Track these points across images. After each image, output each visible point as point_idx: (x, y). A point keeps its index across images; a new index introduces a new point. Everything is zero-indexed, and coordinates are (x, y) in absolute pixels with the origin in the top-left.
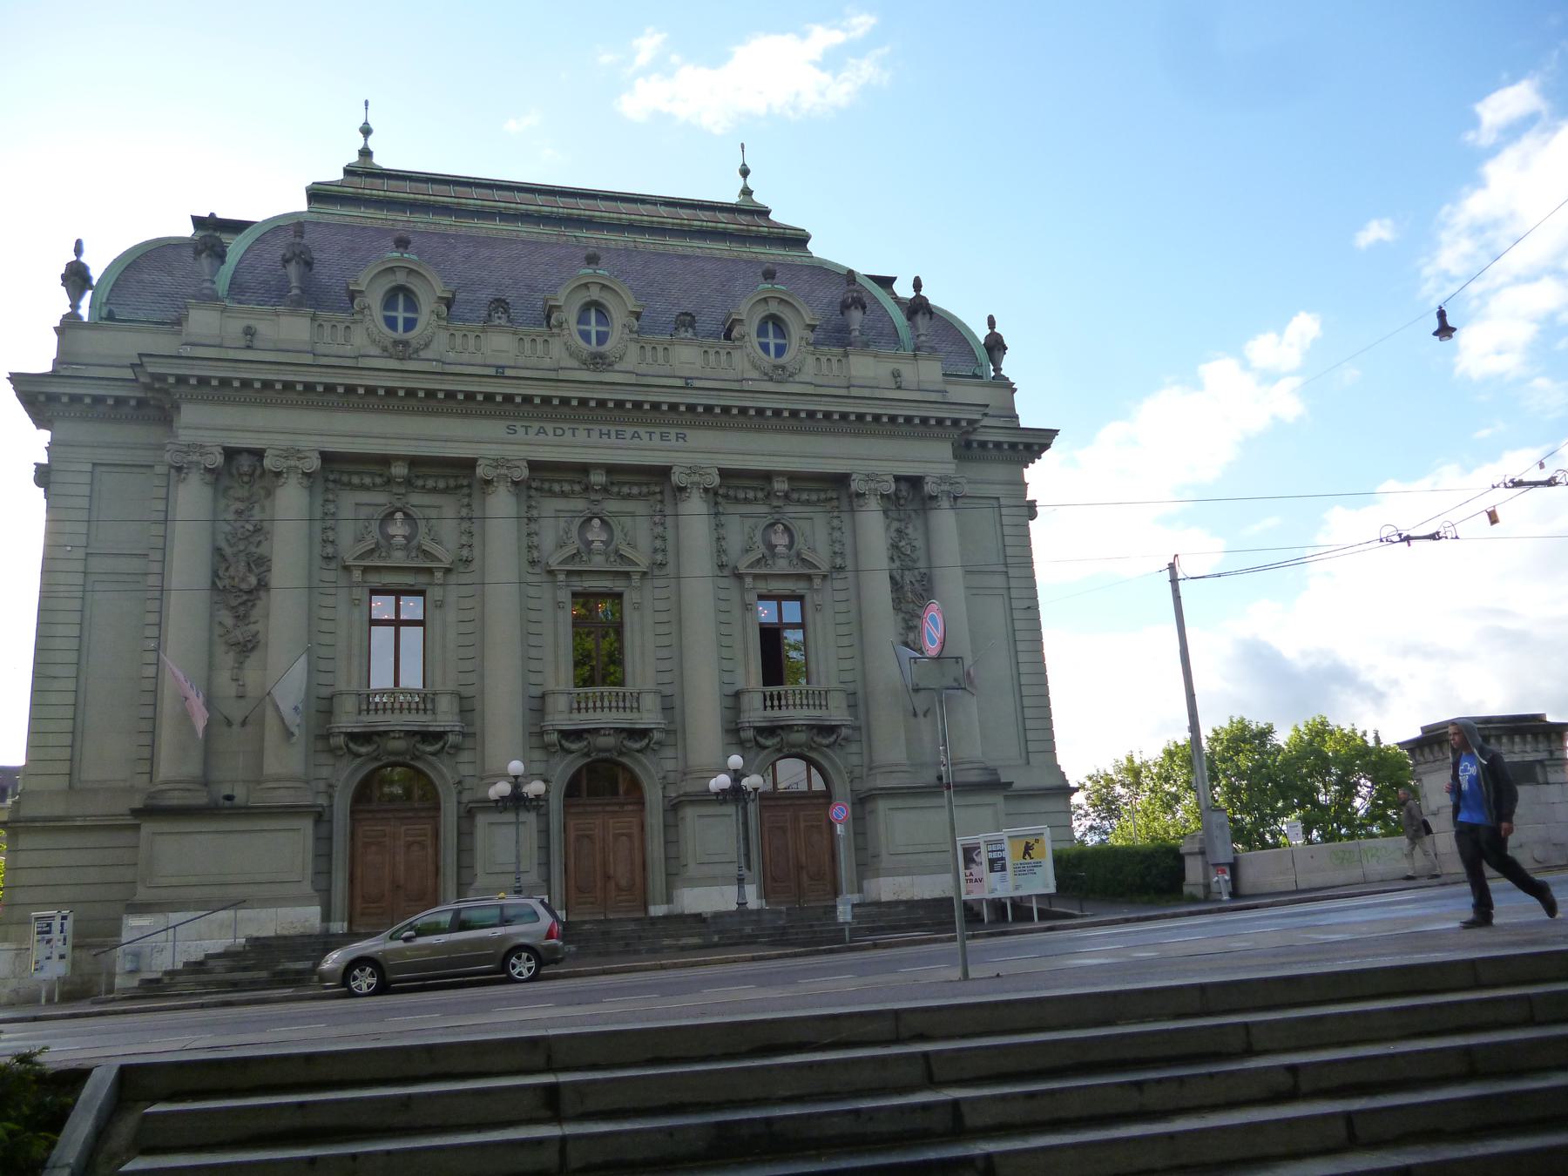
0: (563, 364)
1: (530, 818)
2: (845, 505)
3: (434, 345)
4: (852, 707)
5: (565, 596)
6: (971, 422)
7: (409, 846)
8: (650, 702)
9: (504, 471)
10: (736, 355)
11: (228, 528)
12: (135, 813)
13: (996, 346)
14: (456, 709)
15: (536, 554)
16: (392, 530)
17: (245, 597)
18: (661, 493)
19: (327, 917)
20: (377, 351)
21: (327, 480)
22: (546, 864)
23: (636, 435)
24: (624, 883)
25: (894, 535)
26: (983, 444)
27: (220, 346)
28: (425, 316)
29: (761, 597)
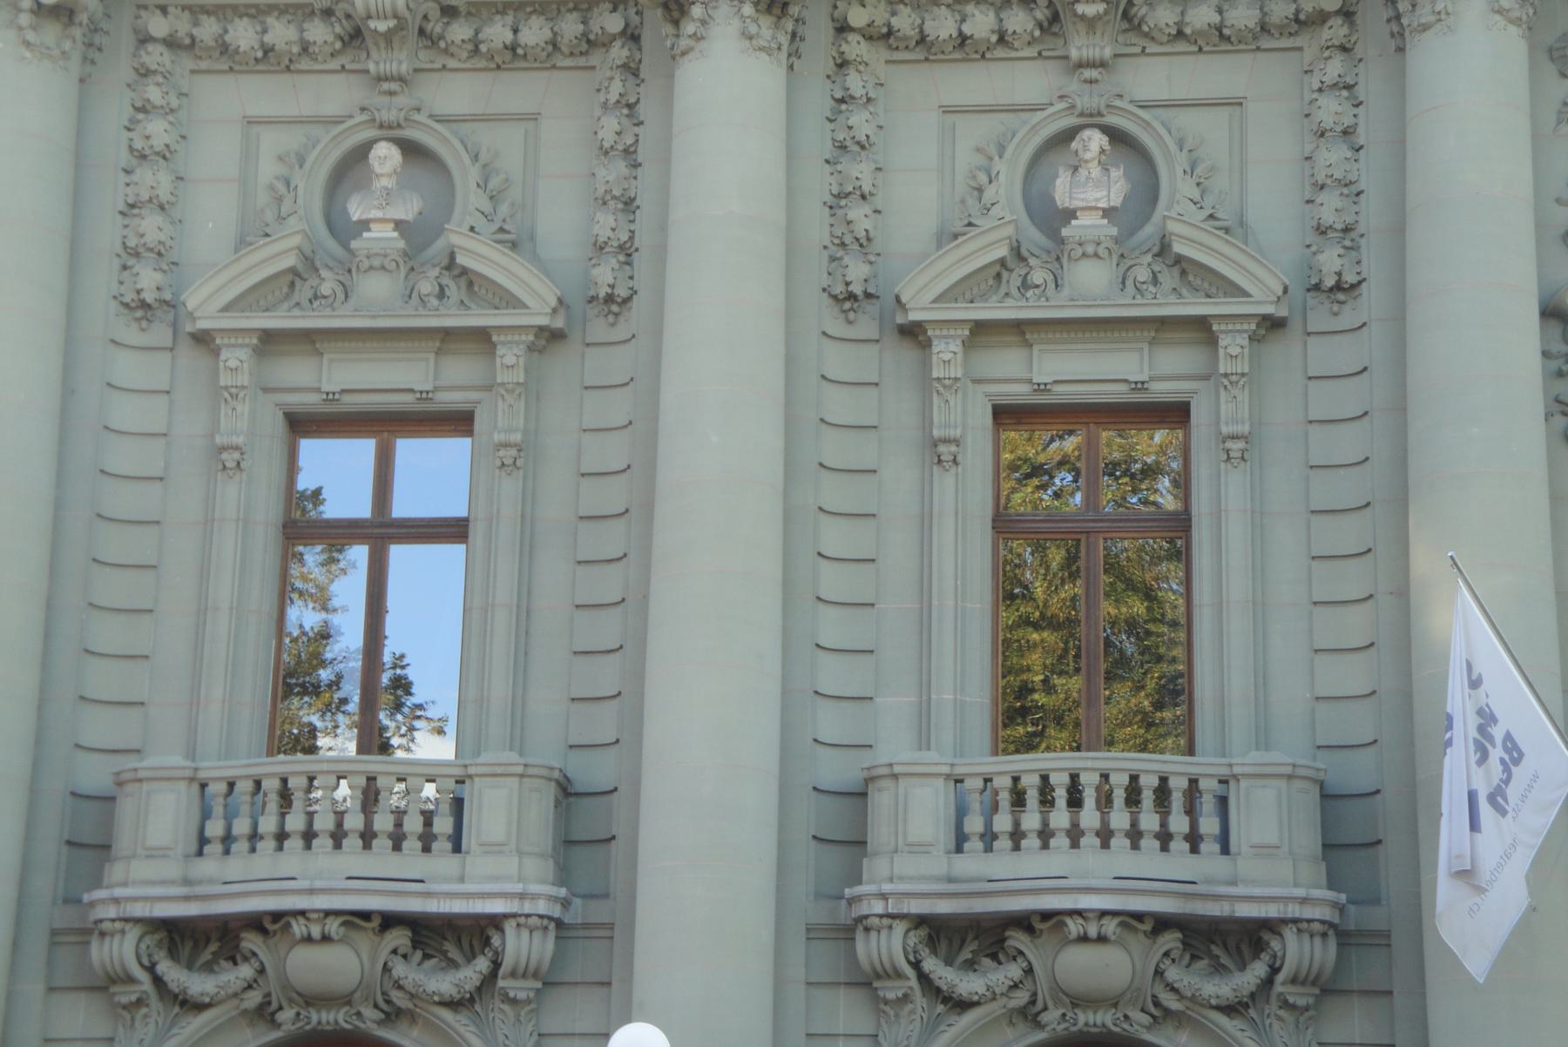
5: (968, 418)
14: (1309, 839)
16: (1063, 191)
18: (632, 36)
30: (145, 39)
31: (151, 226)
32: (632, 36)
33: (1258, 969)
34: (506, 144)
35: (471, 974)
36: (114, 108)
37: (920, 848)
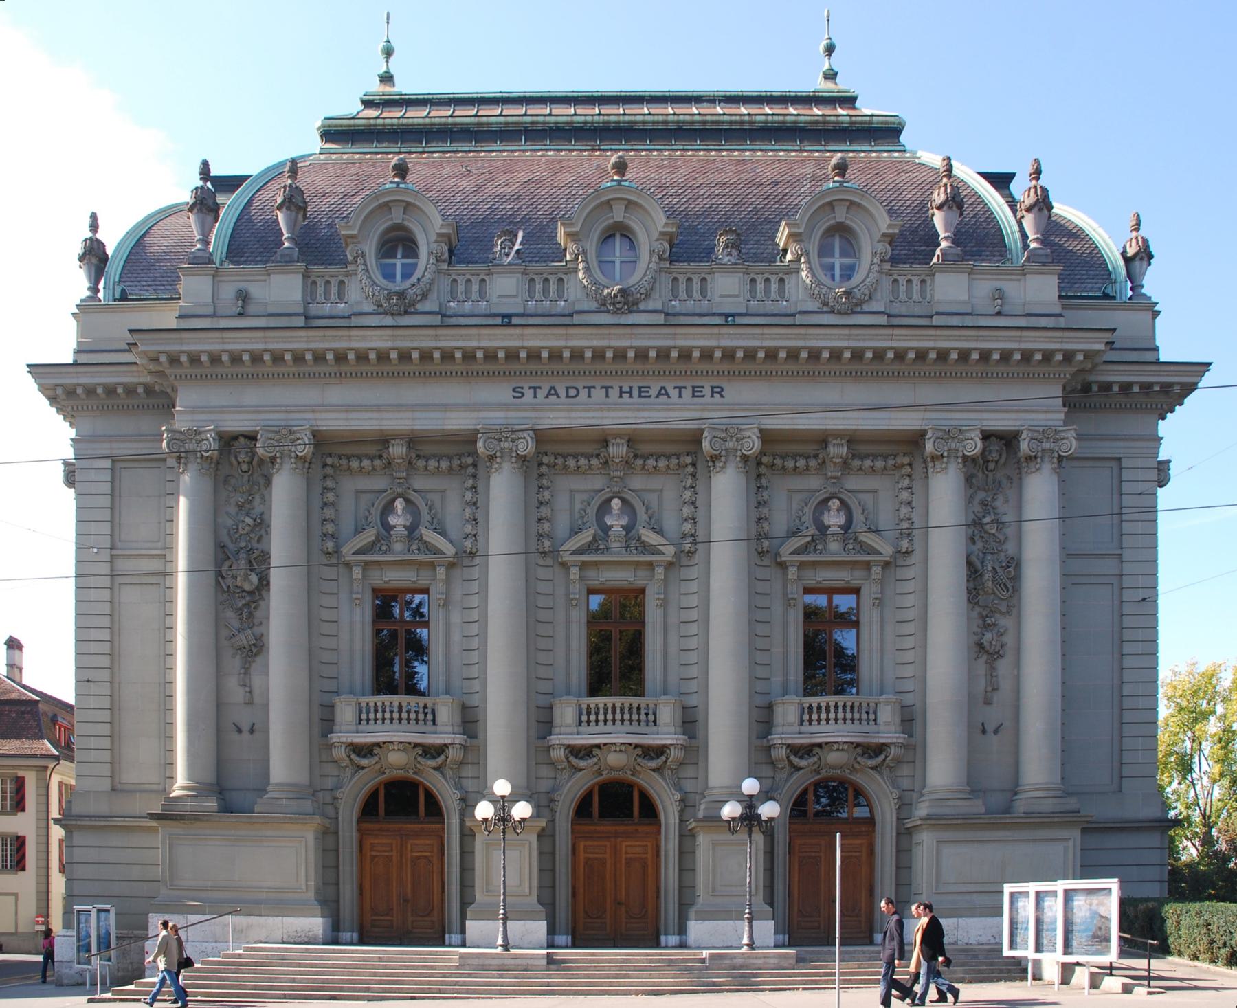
3: (433, 296)
6: (1088, 355)
9: (1047, 445)
11: (229, 522)
14: (458, 719)
23: (663, 392)
25: (977, 508)
26: (1106, 387)
27: (213, 316)
30: (325, 465)
31: (546, 527)
32: (694, 465)
37: (790, 725)
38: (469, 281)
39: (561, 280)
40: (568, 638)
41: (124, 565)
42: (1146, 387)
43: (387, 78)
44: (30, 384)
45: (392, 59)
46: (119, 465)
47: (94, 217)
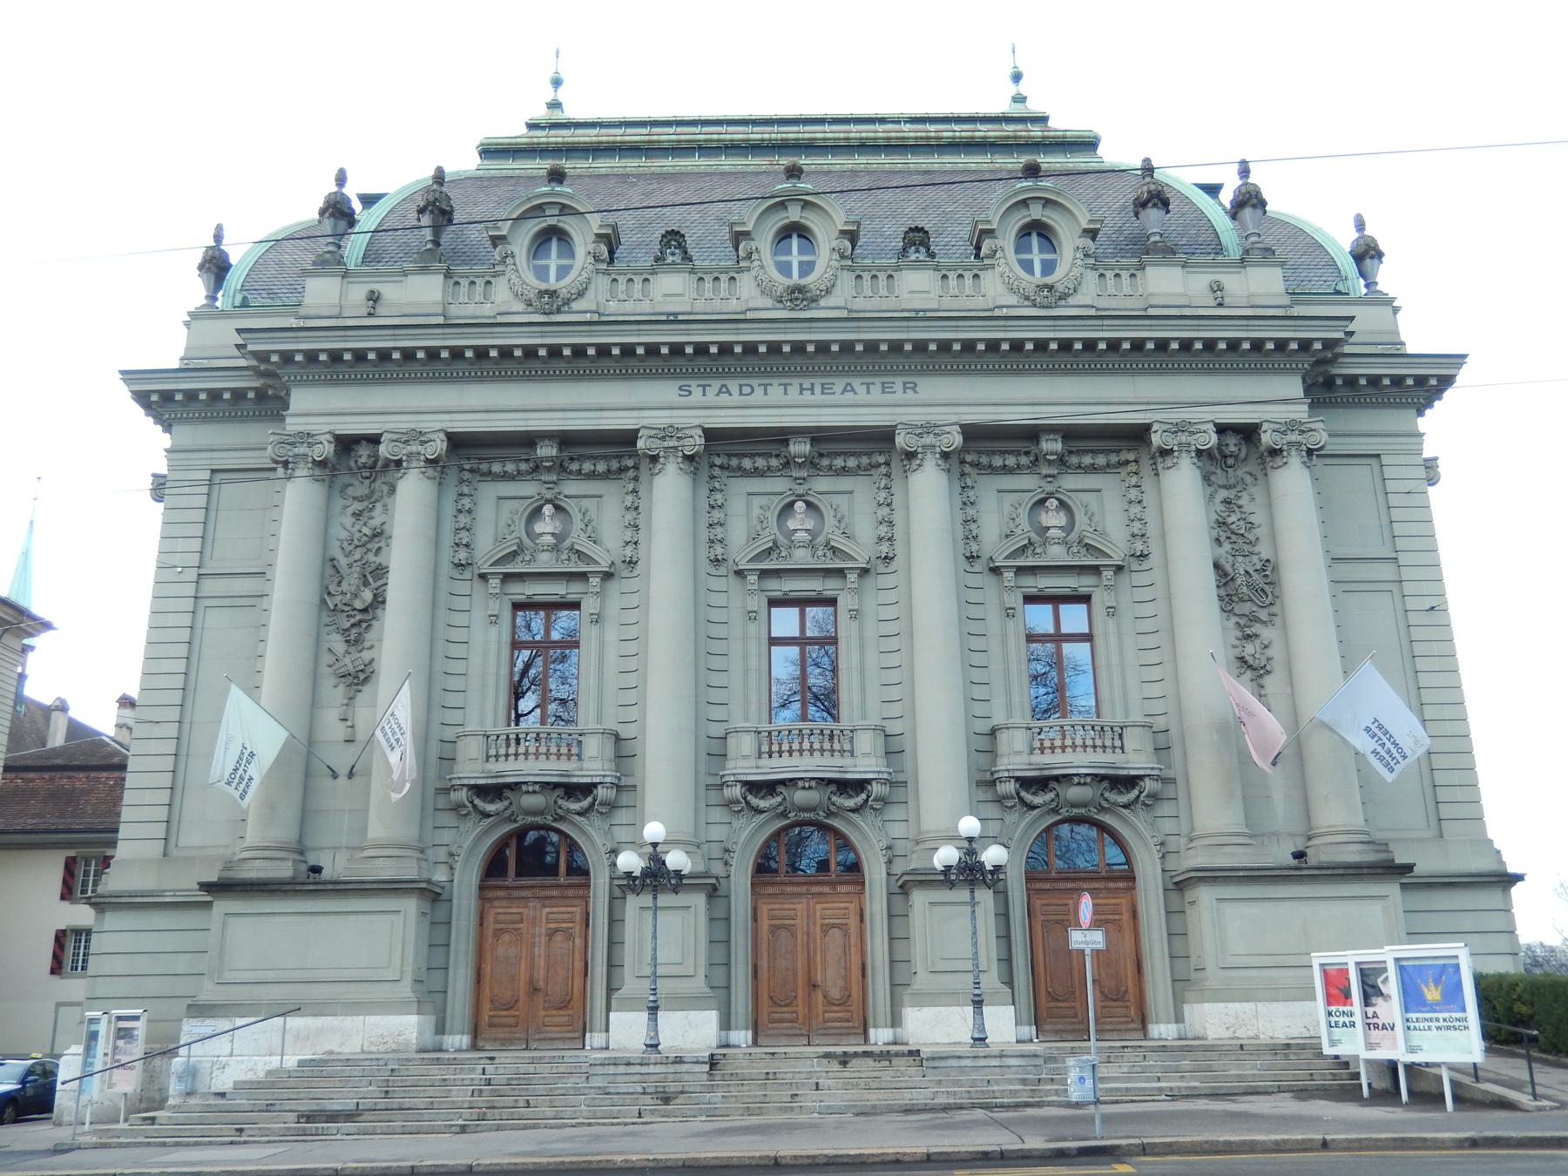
0: (752, 304)
1: (985, 897)
2: (1146, 463)
3: (590, 294)
4: (1161, 750)
6: (1329, 344)
7: (551, 934)
8: (866, 742)
10: (987, 277)
11: (344, 534)
12: (207, 887)
13: (1366, 254)
15: (974, 547)
17: (359, 617)
18: (887, 464)
19: (726, 1024)
20: (520, 307)
21: (962, 462)
22: (1007, 960)
24: (835, 993)
26: (1351, 381)
28: (824, 258)
29: (1029, 599)
30: (712, 466)
32: (887, 464)
33: (864, 796)
34: (841, 501)
35: (585, 803)
36: (451, 494)
37: (1019, 753)
38: (631, 280)
39: (733, 278)
40: (745, 656)
41: (209, 587)
42: (1398, 381)
43: (555, 105)
44: (124, 392)
45: (561, 89)
46: (218, 477)
47: (219, 228)
